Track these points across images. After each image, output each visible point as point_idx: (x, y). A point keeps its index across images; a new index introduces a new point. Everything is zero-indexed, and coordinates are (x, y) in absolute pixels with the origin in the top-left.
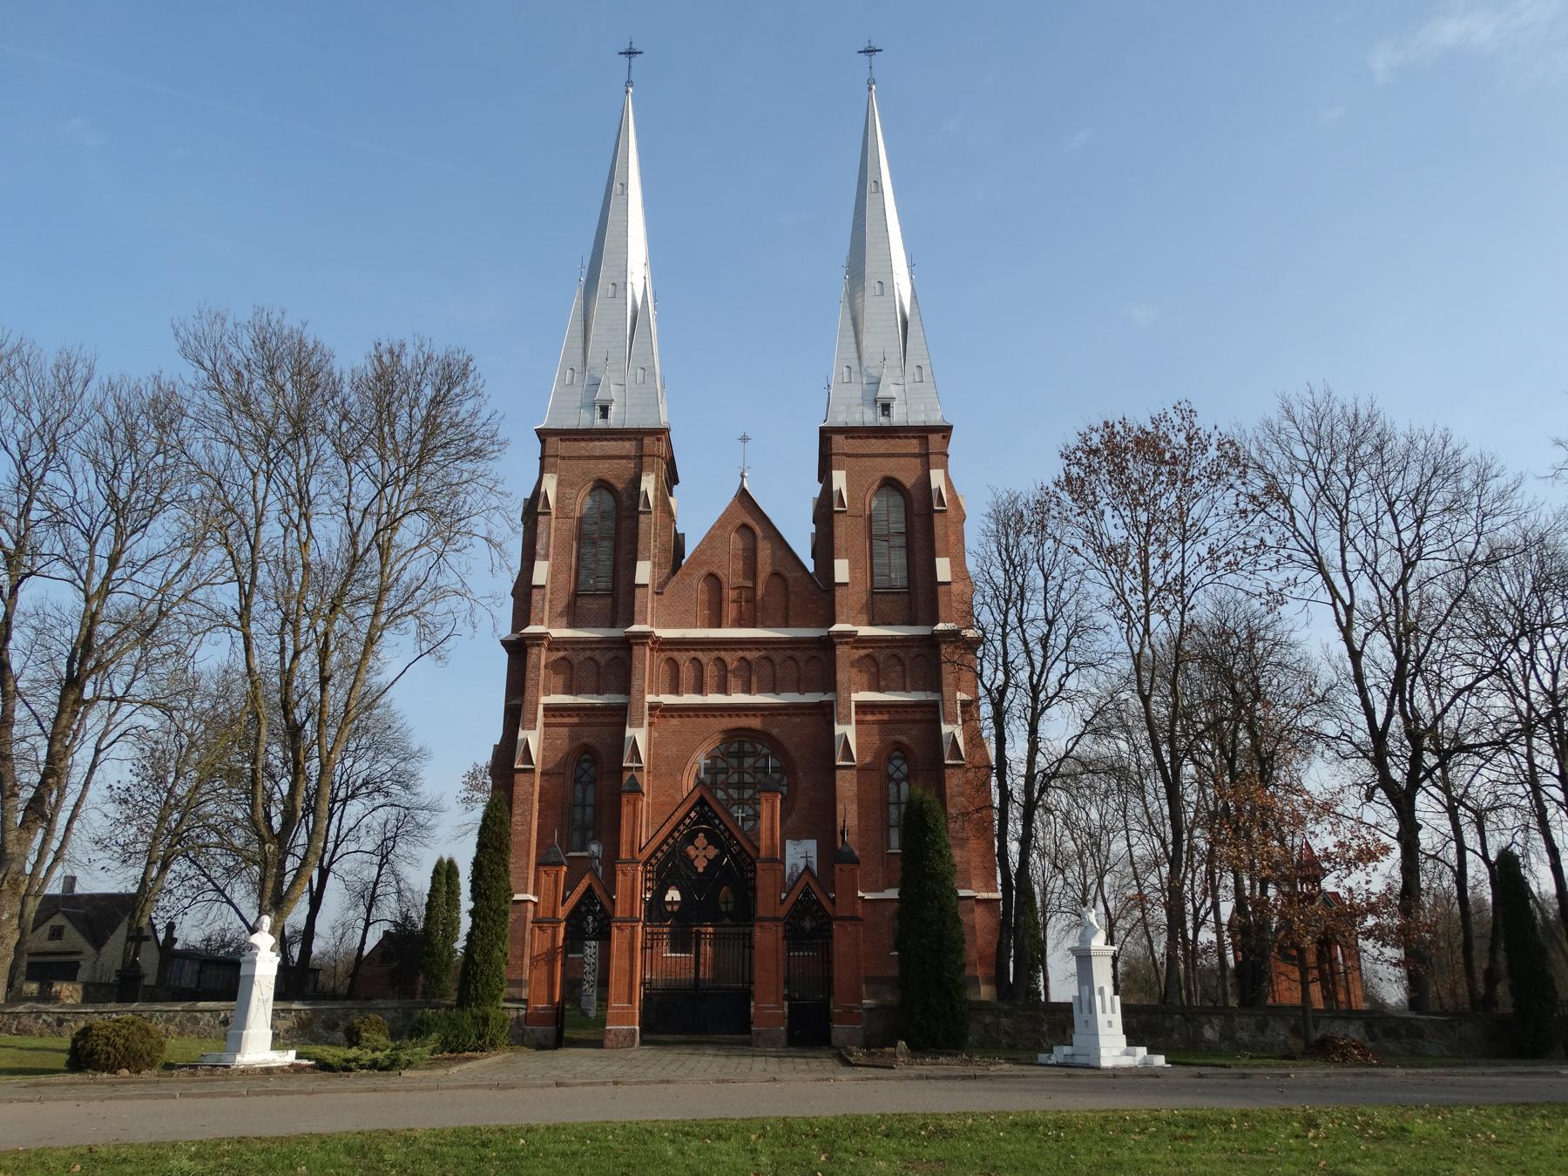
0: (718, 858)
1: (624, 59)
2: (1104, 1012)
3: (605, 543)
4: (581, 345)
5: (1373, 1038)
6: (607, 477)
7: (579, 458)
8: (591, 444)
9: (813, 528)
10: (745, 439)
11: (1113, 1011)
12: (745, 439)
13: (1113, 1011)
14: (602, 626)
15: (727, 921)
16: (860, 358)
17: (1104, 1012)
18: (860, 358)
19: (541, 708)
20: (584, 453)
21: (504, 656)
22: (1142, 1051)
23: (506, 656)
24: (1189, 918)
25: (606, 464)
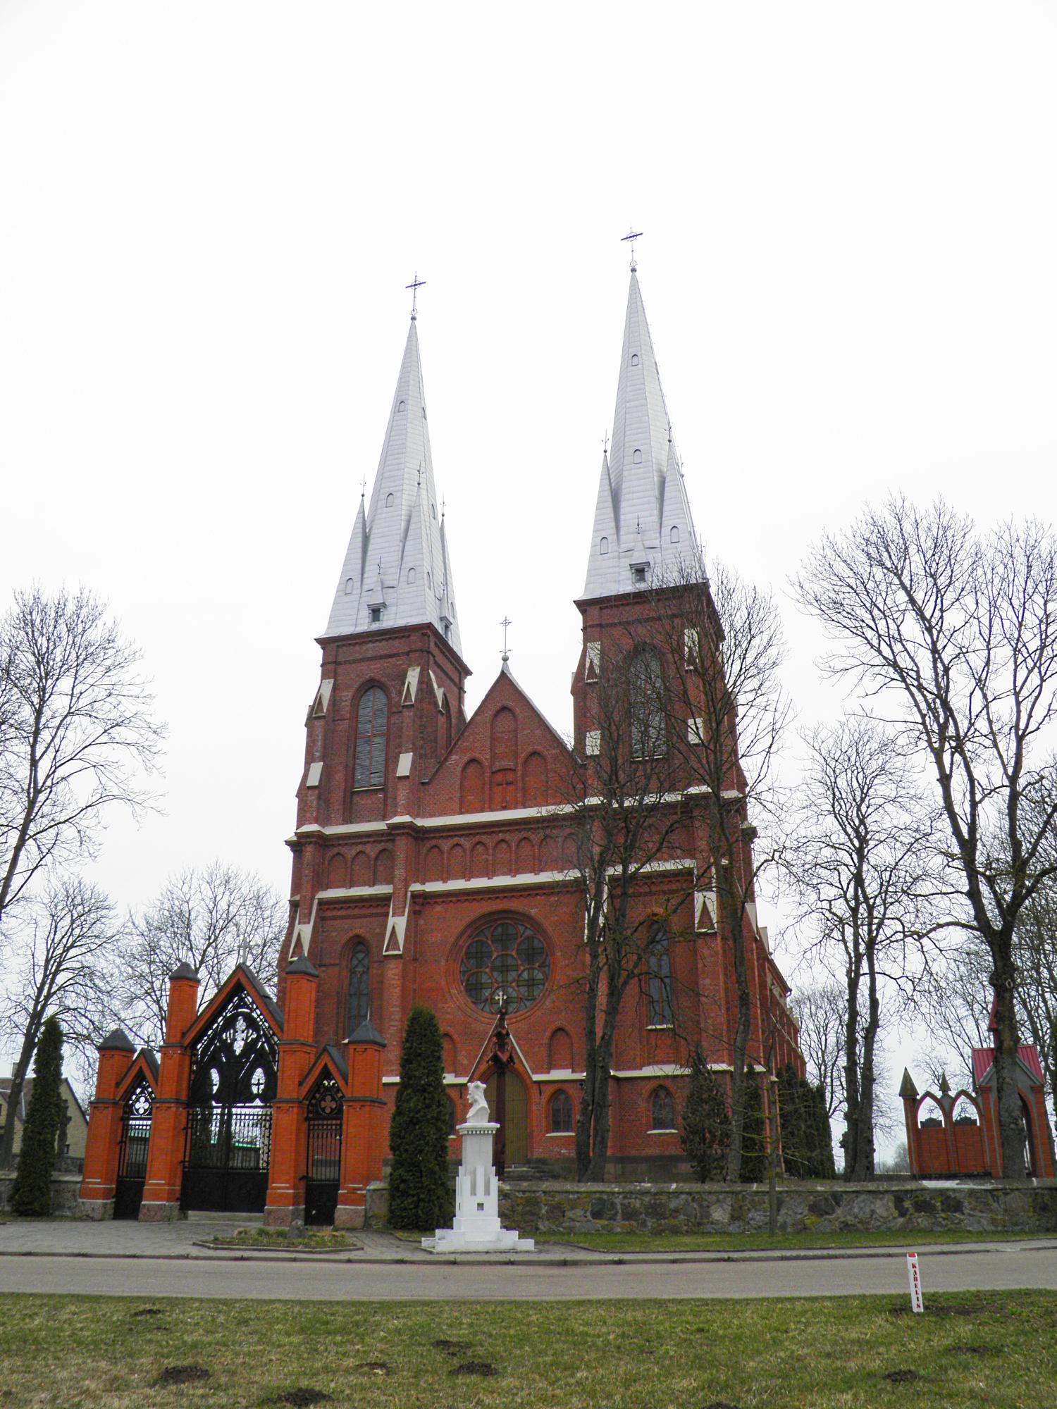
0: (255, 1041)
1: (420, 280)
2: (473, 1193)
3: (377, 740)
4: (360, 555)
5: (903, 1213)
6: (378, 677)
7: (354, 661)
8: (365, 647)
9: (572, 698)
10: (506, 623)
11: (487, 1192)
12: (506, 623)
13: (487, 1192)
14: (376, 820)
15: (258, 1102)
16: (618, 527)
17: (473, 1193)
18: (618, 527)
19: (316, 902)
20: (357, 656)
21: (289, 855)
22: (514, 1234)
23: (291, 854)
24: (23, 1110)
25: (375, 666)
